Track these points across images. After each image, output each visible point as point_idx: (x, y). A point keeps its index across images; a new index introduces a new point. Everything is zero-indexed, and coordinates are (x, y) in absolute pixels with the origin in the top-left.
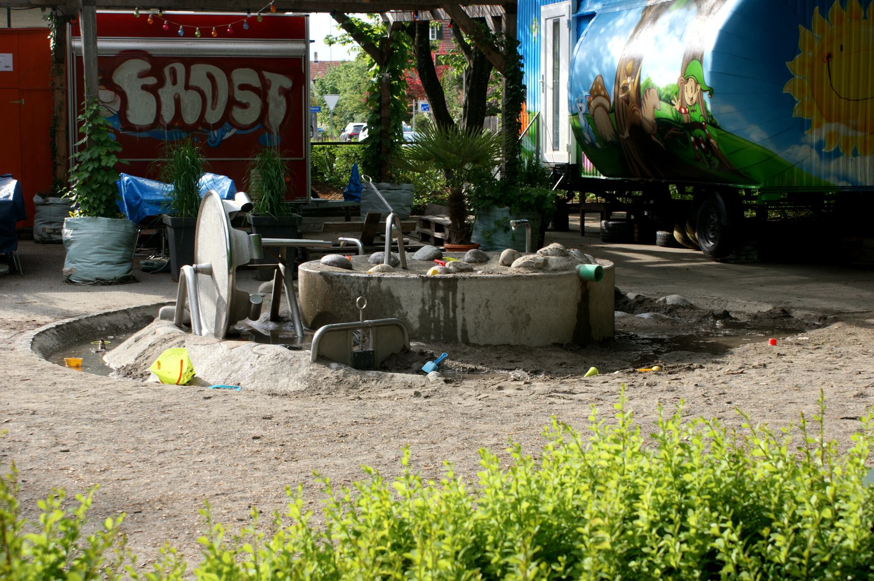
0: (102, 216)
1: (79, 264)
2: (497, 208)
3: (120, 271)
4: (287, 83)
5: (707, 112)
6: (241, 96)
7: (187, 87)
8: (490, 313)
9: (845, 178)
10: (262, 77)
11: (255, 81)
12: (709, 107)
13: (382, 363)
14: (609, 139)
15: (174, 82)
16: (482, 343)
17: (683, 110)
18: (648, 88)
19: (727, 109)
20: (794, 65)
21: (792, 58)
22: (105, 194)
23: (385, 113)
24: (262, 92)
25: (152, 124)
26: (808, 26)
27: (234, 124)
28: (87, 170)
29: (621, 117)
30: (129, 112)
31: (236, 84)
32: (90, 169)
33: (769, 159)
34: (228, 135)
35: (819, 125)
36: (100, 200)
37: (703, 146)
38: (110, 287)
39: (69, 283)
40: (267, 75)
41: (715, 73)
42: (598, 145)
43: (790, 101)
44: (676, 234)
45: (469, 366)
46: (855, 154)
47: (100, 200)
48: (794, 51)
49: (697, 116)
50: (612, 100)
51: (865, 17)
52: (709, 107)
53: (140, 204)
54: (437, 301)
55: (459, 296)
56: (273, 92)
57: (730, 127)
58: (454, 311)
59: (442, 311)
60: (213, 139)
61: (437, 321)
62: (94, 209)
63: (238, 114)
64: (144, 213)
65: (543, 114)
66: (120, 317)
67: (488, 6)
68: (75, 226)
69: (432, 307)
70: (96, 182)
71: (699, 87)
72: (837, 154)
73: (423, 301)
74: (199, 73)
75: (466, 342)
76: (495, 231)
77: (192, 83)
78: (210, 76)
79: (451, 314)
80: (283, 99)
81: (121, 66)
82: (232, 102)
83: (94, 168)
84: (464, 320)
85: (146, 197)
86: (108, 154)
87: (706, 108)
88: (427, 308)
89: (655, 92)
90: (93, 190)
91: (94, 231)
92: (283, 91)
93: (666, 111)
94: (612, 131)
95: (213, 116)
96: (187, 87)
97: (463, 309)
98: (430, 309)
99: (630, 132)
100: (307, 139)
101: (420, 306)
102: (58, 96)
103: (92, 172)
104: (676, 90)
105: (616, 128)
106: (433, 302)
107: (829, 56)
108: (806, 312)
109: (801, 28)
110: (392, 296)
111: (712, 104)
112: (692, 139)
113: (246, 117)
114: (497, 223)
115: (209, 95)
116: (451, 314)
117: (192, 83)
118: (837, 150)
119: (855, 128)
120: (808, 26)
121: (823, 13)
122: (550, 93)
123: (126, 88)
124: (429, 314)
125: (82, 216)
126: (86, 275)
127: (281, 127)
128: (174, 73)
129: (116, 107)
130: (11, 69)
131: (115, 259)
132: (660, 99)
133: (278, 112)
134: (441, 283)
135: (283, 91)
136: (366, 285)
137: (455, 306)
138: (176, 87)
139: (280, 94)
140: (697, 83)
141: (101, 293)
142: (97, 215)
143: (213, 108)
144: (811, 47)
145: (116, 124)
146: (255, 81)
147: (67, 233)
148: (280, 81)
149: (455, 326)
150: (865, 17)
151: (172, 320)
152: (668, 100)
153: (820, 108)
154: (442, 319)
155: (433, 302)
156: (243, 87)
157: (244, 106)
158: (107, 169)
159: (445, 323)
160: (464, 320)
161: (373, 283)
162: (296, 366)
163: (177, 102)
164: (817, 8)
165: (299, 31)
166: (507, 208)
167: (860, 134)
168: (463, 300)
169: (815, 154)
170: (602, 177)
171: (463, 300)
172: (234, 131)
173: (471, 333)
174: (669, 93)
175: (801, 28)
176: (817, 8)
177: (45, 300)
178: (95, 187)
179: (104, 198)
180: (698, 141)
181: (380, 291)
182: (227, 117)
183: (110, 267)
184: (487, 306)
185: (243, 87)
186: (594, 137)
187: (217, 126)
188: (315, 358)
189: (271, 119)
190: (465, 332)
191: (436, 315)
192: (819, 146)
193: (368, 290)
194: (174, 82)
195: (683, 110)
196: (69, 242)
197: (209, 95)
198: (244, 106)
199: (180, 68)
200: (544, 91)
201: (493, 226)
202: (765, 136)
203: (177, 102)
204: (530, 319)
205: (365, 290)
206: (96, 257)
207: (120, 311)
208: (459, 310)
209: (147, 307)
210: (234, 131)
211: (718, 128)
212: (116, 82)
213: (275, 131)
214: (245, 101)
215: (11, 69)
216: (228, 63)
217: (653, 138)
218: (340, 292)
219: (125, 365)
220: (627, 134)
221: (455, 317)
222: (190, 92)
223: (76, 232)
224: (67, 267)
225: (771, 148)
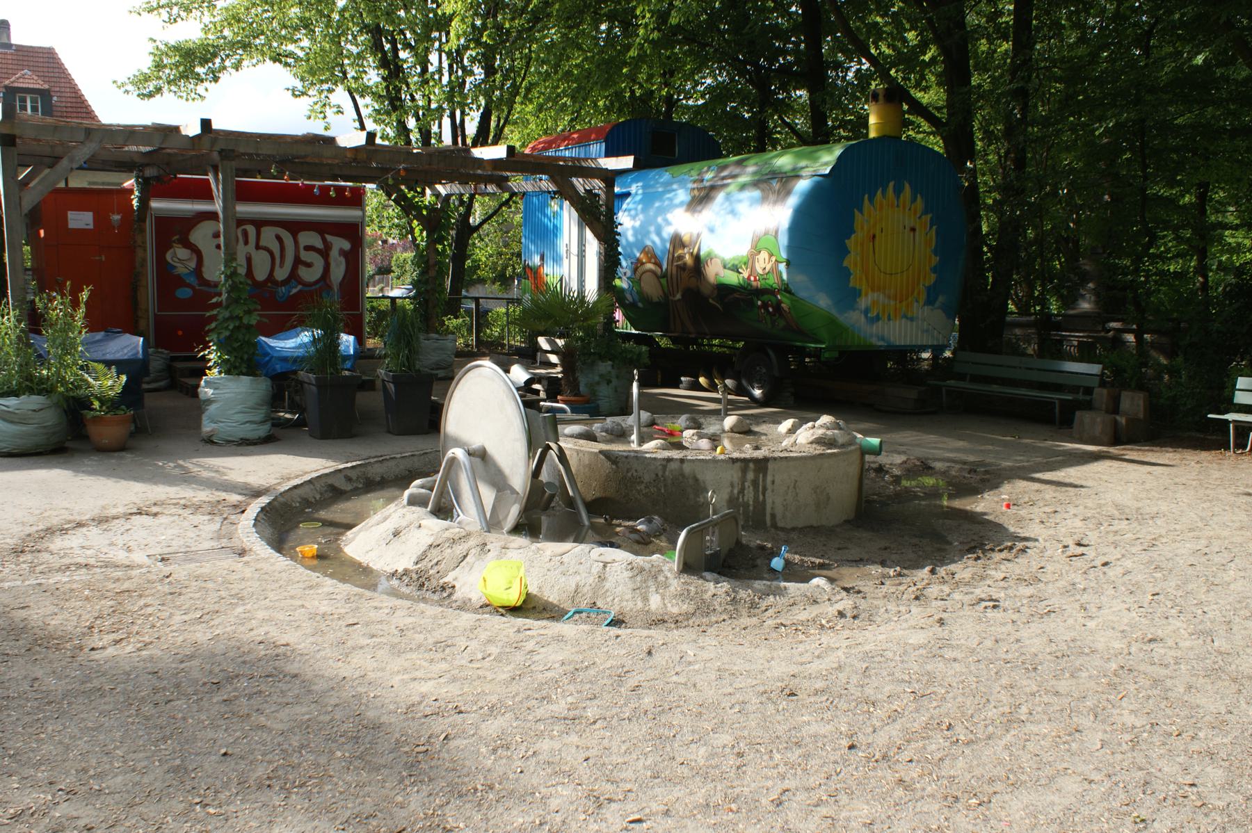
0: (244, 374)
1: (221, 424)
2: (600, 363)
3: (263, 430)
4: (346, 245)
5: (783, 280)
6: (305, 256)
7: (258, 247)
8: (797, 494)
9: (883, 339)
10: (324, 240)
11: (318, 243)
12: (785, 277)
13: (724, 561)
14: (655, 299)
15: (246, 243)
16: (789, 527)
17: (752, 278)
18: (710, 256)
19: (800, 278)
20: (851, 243)
21: (849, 238)
22: (246, 353)
23: (432, 273)
24: (325, 253)
25: (203, 278)
26: (861, 211)
27: (300, 281)
28: (227, 328)
29: (675, 280)
30: (204, 269)
31: (301, 247)
32: (231, 327)
33: (832, 322)
34: (294, 291)
35: (866, 295)
36: (242, 358)
37: (771, 309)
38: (251, 448)
39: (214, 444)
40: (329, 238)
41: (791, 248)
42: (640, 305)
43: (846, 274)
44: (702, 380)
45: (817, 561)
46: (889, 319)
47: (242, 358)
48: (850, 231)
49: (772, 281)
50: (665, 267)
51: (898, 206)
52: (785, 277)
53: (270, 360)
54: (747, 484)
55: (769, 479)
56: (334, 253)
57: (803, 294)
58: (764, 495)
59: (752, 495)
60: (281, 294)
61: (746, 505)
62: (235, 368)
63: (303, 273)
64: (274, 370)
65: (566, 275)
66: (307, 488)
67: (580, 180)
68: (215, 386)
69: (742, 491)
70: (237, 340)
71: (774, 259)
72: (877, 318)
73: (732, 485)
74: (268, 235)
75: (774, 525)
76: (598, 383)
77: (262, 243)
78: (279, 238)
79: (761, 497)
80: (342, 260)
81: (199, 226)
82: (298, 262)
83: (235, 327)
84: (773, 503)
85: (276, 355)
86: (249, 312)
87: (781, 277)
88: (736, 491)
89: (719, 261)
90: (235, 349)
91: (237, 390)
92: (342, 252)
93: (731, 278)
94: (661, 293)
95: (281, 274)
96: (258, 247)
97: (773, 491)
98: (739, 493)
99: (683, 296)
100: (364, 293)
101: (729, 490)
102: (139, 252)
103: (232, 331)
104: (745, 260)
105: (666, 290)
106: (743, 484)
107: (874, 237)
108: (948, 464)
109: (856, 212)
110: (696, 480)
111: (788, 273)
112: (759, 303)
113: (310, 275)
114: (601, 376)
115: (277, 255)
116: (761, 497)
117: (262, 243)
118: (878, 315)
119: (889, 297)
120: (861, 211)
121: (871, 200)
122: (574, 260)
123: (201, 247)
124: (738, 498)
125: (223, 375)
126: (230, 436)
127: (341, 284)
128: (245, 234)
129: (193, 265)
130: (91, 227)
131: (258, 418)
132: (725, 267)
133: (338, 272)
134: (751, 465)
135: (342, 252)
136: (664, 467)
137: (765, 489)
138: (247, 247)
139: (340, 255)
140: (771, 255)
141: (262, 458)
142: (238, 375)
143: (281, 266)
144: (862, 228)
145: (192, 280)
146: (318, 243)
147: (206, 391)
148: (340, 244)
149: (764, 509)
150: (898, 206)
151: (426, 507)
152: (736, 269)
153: (867, 279)
154: (751, 503)
155: (743, 484)
156: (307, 248)
157: (309, 265)
158: (249, 327)
159: (754, 507)
160: (773, 503)
161: (673, 466)
162: (661, 578)
163: (249, 260)
164: (866, 196)
165: (357, 199)
166: (610, 363)
167: (892, 303)
168: (773, 482)
169: (863, 319)
170: (634, 331)
171: (773, 482)
172: (300, 287)
173: (779, 516)
174: (736, 262)
175: (856, 212)
176: (866, 196)
177: (209, 469)
178: (236, 345)
179: (246, 357)
180: (765, 306)
181: (683, 475)
182: (293, 275)
183: (254, 426)
184: (794, 487)
185: (307, 248)
186: (636, 298)
187: (285, 282)
188: (681, 567)
189: (332, 278)
190: (773, 516)
191: (746, 499)
192: (866, 311)
193: (667, 473)
194: (246, 243)
195: (752, 278)
196: (209, 401)
197: (277, 255)
198: (309, 265)
199: (251, 230)
200: (568, 257)
201: (597, 378)
202: (829, 302)
203: (249, 260)
204: (829, 498)
205: (664, 472)
206: (239, 417)
207: (305, 482)
208: (768, 493)
209: (326, 475)
210: (300, 287)
211: (793, 294)
212: (192, 241)
213: (336, 288)
214: (309, 261)
215: (91, 227)
216: (295, 227)
217: (711, 301)
218: (629, 474)
219: (400, 570)
220: (678, 296)
221: (764, 500)
222: (261, 251)
223: (217, 391)
224: (207, 427)
225: (834, 312)
